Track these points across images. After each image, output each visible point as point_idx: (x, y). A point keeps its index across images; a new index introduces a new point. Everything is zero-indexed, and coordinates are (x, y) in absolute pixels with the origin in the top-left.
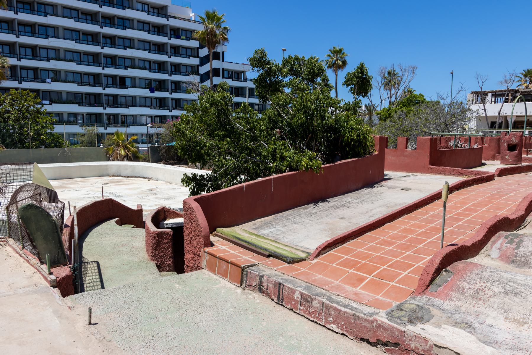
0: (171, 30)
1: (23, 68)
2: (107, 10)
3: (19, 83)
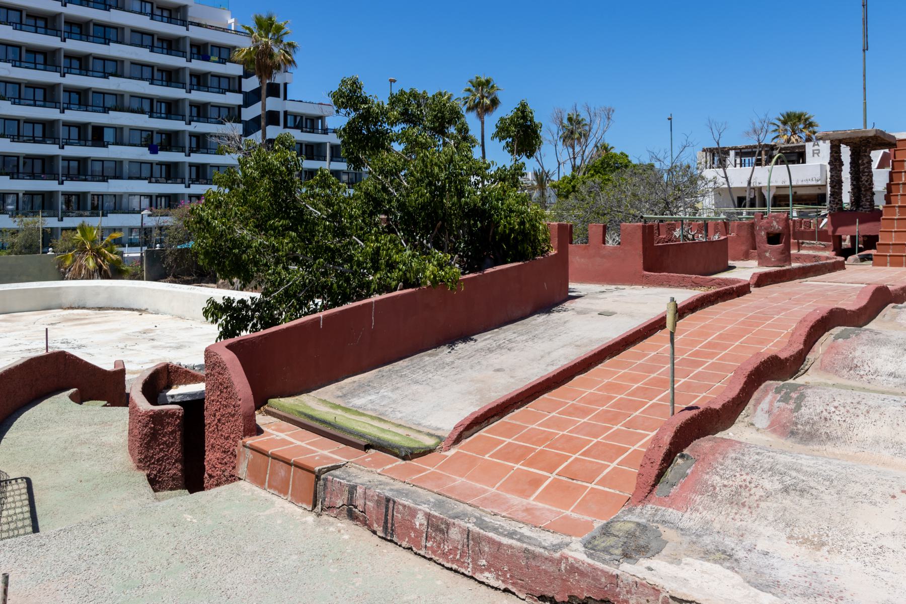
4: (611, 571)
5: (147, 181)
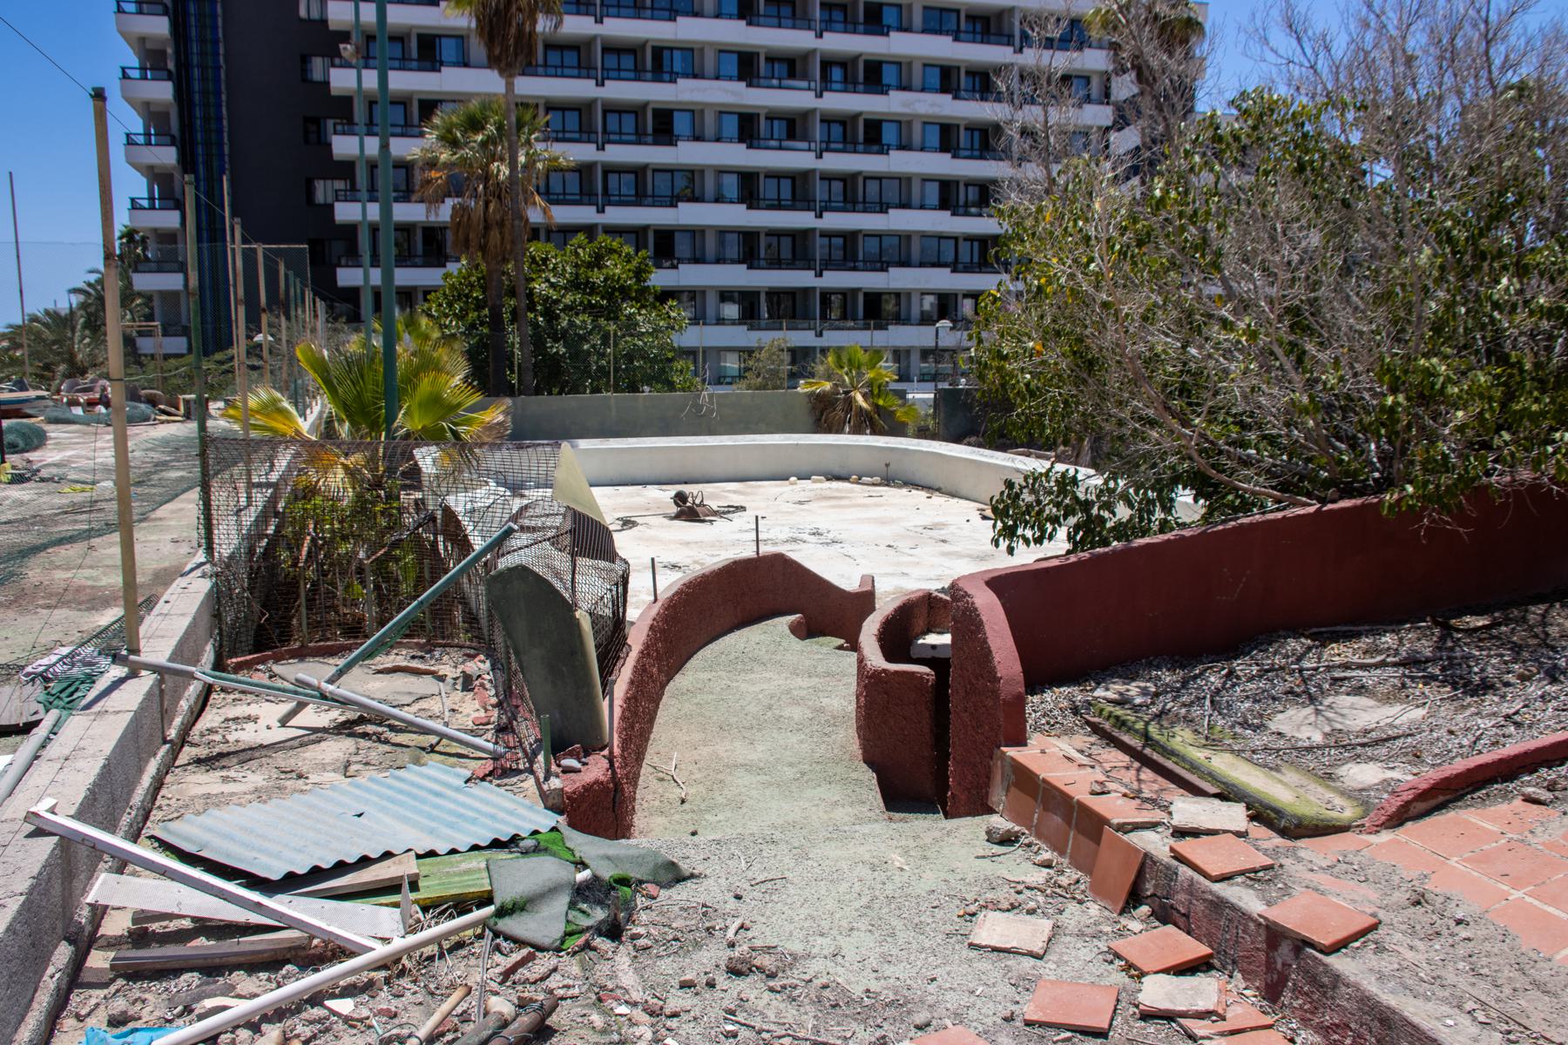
1: (610, 170)
3: (598, 212)
5: (949, 270)
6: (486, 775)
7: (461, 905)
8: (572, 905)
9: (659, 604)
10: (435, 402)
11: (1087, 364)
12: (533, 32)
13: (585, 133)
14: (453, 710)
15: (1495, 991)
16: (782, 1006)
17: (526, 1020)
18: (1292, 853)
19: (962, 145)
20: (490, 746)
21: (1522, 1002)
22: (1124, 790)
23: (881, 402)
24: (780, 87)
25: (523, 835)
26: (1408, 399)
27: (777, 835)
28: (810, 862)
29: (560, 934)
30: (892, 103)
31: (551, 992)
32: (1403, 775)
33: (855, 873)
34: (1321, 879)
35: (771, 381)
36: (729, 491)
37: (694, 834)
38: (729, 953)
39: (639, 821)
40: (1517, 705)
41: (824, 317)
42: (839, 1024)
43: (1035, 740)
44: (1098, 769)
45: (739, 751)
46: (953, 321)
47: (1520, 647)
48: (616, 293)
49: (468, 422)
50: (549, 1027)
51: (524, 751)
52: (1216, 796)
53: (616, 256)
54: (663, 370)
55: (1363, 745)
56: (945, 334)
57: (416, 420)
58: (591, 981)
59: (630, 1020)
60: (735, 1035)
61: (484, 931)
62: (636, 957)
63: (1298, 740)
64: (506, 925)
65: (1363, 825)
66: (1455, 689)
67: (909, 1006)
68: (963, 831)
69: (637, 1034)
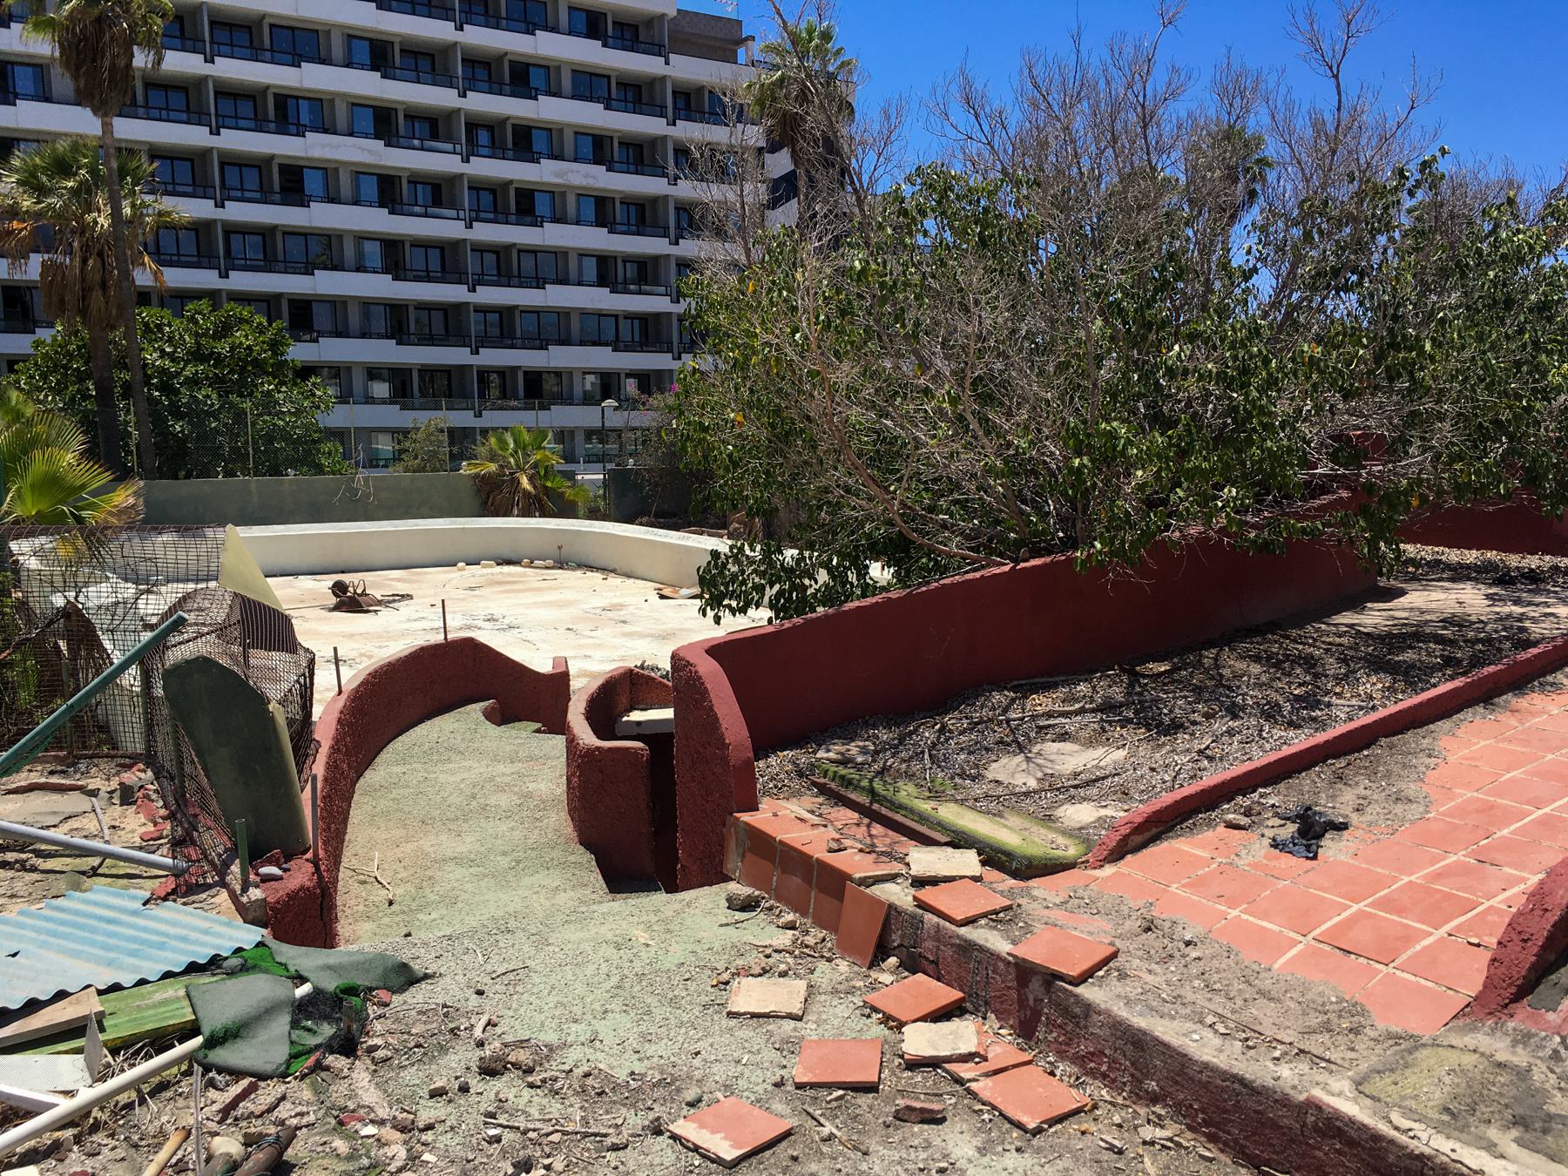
0: (212, 23)
2: (479, 37)
4: (1412, 1147)
6: (168, 894)
7: (159, 1041)
8: (295, 1024)
9: (344, 697)
10: (52, 484)
11: (783, 434)
12: (129, 65)
13: (199, 188)
14: (114, 827)
15: (1229, 1004)
16: (545, 1101)
17: (260, 1156)
18: (1027, 893)
19: (618, 220)
20: (169, 861)
21: (1253, 1011)
22: (860, 846)
23: (549, 484)
24: (422, 149)
25: (225, 954)
26: (1091, 460)
27: (512, 924)
28: (551, 948)
29: (285, 1057)
30: (544, 172)
31: (282, 1123)
32: (1114, 811)
33: (601, 953)
34: (1056, 915)
35: (429, 463)
36: (392, 579)
37: (408, 935)
38: (479, 1053)
39: (343, 928)
40: (1207, 741)
41: (482, 396)
42: (607, 1112)
43: (765, 804)
44: (830, 828)
45: (448, 845)
46: (618, 399)
47: (1200, 688)
48: (248, 368)
49: (92, 506)
50: (286, 1163)
51: (212, 863)
52: (947, 844)
53: (246, 327)
54: (308, 453)
55: (1076, 787)
56: (610, 413)
57: (29, 504)
58: (328, 1104)
59: (379, 1140)
60: (498, 1139)
61: (191, 1066)
62: (375, 1071)
63: (1015, 786)
64: (221, 1055)
65: (1088, 861)
66: (1150, 730)
67: (678, 1083)
68: (702, 901)
69: (390, 1154)
